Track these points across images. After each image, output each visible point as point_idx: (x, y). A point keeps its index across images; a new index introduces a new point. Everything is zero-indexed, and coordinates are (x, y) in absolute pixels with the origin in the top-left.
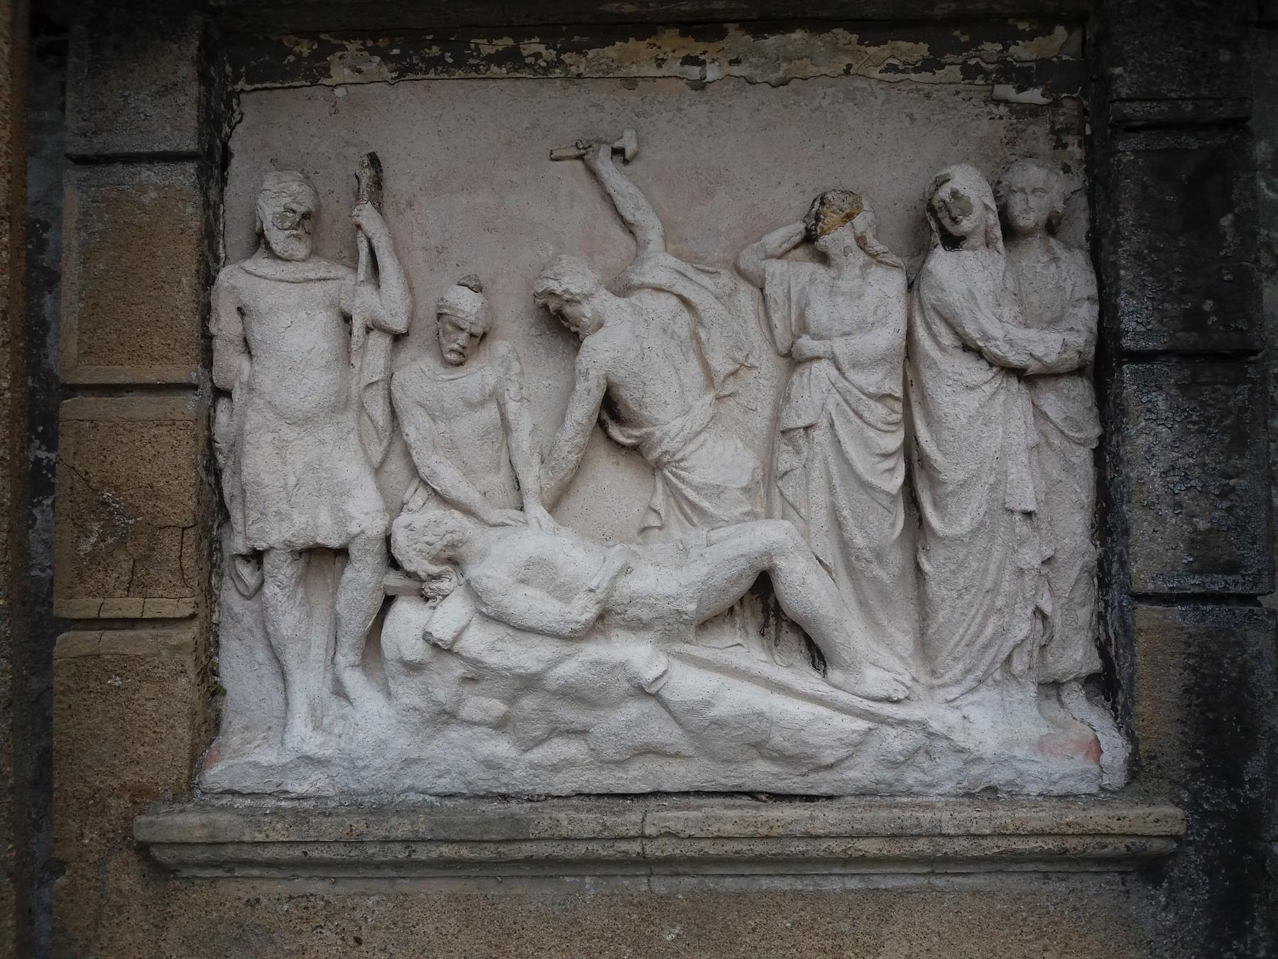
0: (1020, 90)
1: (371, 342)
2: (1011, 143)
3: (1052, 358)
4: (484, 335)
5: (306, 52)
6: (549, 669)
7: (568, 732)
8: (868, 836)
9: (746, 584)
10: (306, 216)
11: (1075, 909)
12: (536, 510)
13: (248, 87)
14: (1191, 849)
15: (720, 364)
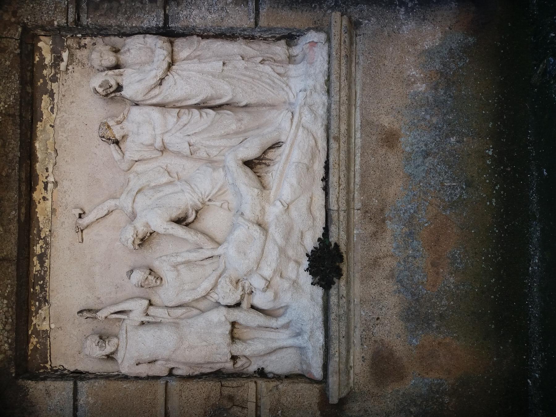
0: (62, 60)
1: (152, 314)
2: (83, 65)
3: (165, 53)
4: (151, 270)
5: (36, 340)
6: (277, 244)
7: (302, 238)
8: (339, 128)
9: (248, 170)
10: (101, 338)
11: (369, 53)
12: (220, 251)
13: (49, 363)
14: (349, 10)
15: (165, 179)
